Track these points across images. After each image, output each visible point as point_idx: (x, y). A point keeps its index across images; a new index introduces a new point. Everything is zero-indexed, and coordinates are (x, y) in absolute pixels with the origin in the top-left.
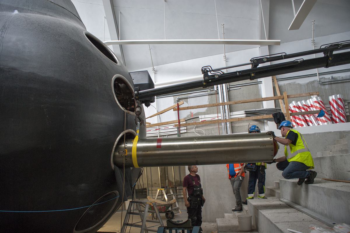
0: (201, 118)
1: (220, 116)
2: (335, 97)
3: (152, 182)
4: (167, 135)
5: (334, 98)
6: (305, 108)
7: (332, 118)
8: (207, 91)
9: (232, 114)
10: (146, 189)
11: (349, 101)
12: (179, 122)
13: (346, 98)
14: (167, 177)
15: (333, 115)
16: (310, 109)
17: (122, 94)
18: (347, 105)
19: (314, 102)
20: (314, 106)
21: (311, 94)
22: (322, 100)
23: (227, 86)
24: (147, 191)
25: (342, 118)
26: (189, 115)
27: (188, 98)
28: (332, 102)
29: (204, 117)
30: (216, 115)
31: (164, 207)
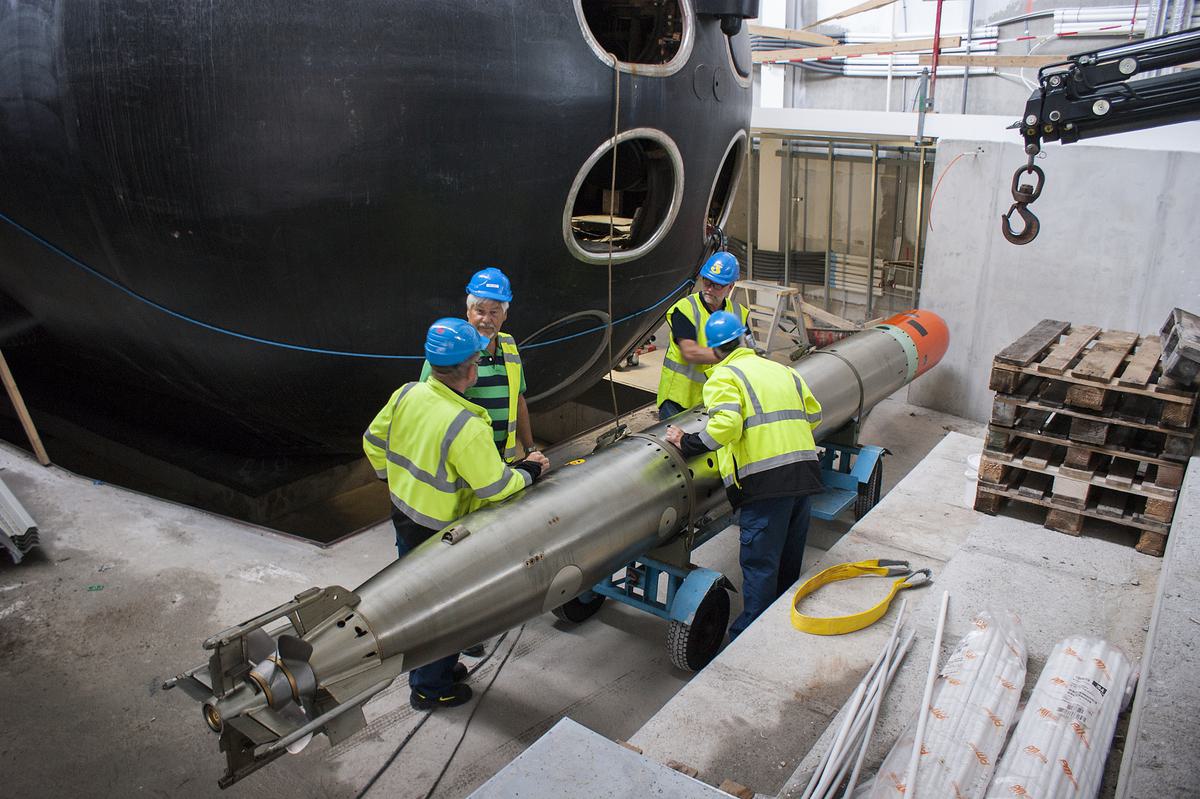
0: (1063, 22)
1: (1146, 15)
3: (849, 235)
10: (823, 255)
14: (899, 229)
24: (826, 264)
29: (1075, 17)
30: (1127, 12)
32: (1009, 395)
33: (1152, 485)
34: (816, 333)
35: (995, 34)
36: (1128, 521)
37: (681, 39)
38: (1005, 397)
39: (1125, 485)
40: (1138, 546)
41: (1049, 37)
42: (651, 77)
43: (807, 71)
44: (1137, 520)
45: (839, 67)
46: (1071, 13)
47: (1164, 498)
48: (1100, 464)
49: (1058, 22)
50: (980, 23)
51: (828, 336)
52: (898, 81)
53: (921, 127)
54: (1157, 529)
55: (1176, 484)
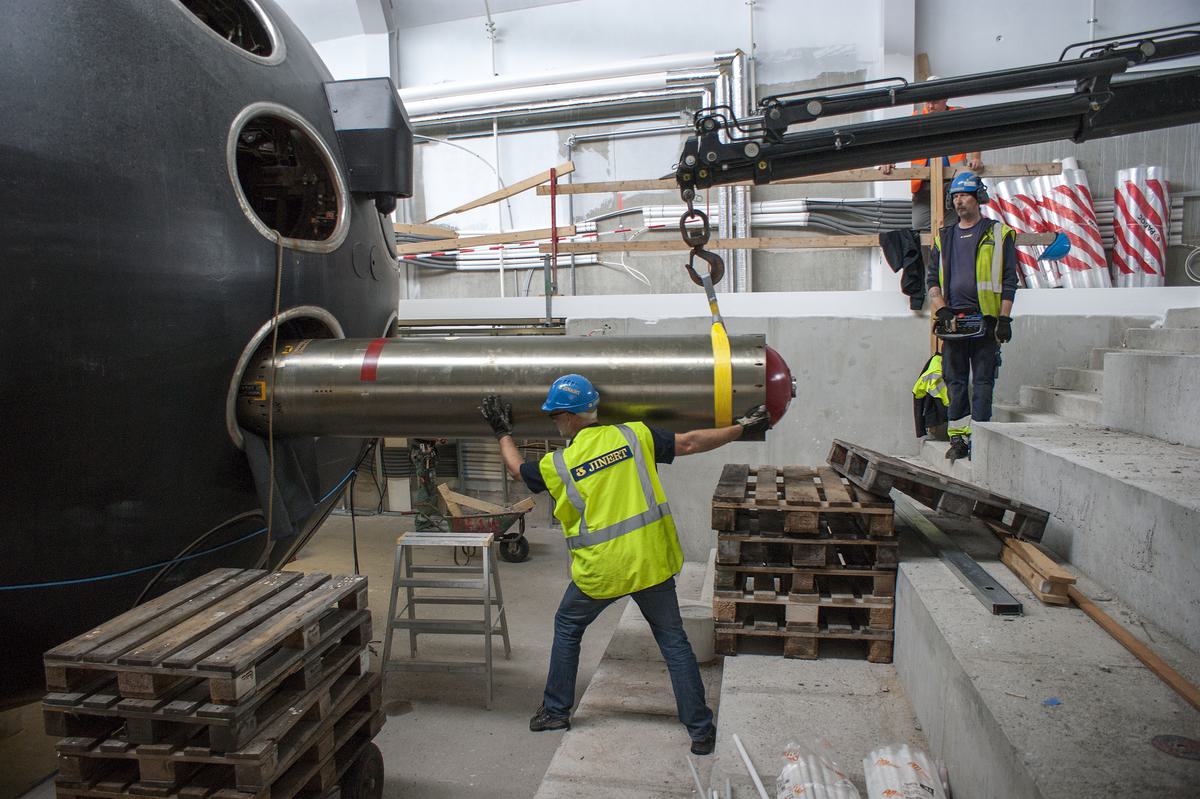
0: (651, 217)
1: (716, 212)
2: (1138, 174)
4: (531, 268)
5: (1134, 181)
6: (1021, 210)
7: (1111, 253)
8: (678, 118)
9: (759, 210)
11: (1196, 193)
12: (556, 239)
13: (1184, 181)
15: (1119, 242)
16: (1038, 211)
17: (299, 165)
18: (1179, 207)
19: (1056, 188)
20: (1055, 203)
21: (1031, 169)
22: (1086, 185)
23: (750, 104)
25: (1148, 256)
26: (609, 202)
27: (607, 140)
28: (1124, 193)
29: (660, 213)
31: (493, 523)
32: (731, 532)
33: (872, 597)
34: (466, 520)
35: (594, 228)
36: (858, 635)
37: (336, 218)
38: (728, 535)
39: (849, 601)
40: (870, 657)
41: (641, 230)
42: (313, 253)
43: (420, 267)
44: (866, 632)
45: (451, 263)
46: (657, 210)
47: (884, 606)
48: (825, 585)
49: (647, 217)
50: (580, 219)
51: (478, 522)
52: (509, 274)
53: (549, 310)
54: (884, 637)
55: (890, 591)
